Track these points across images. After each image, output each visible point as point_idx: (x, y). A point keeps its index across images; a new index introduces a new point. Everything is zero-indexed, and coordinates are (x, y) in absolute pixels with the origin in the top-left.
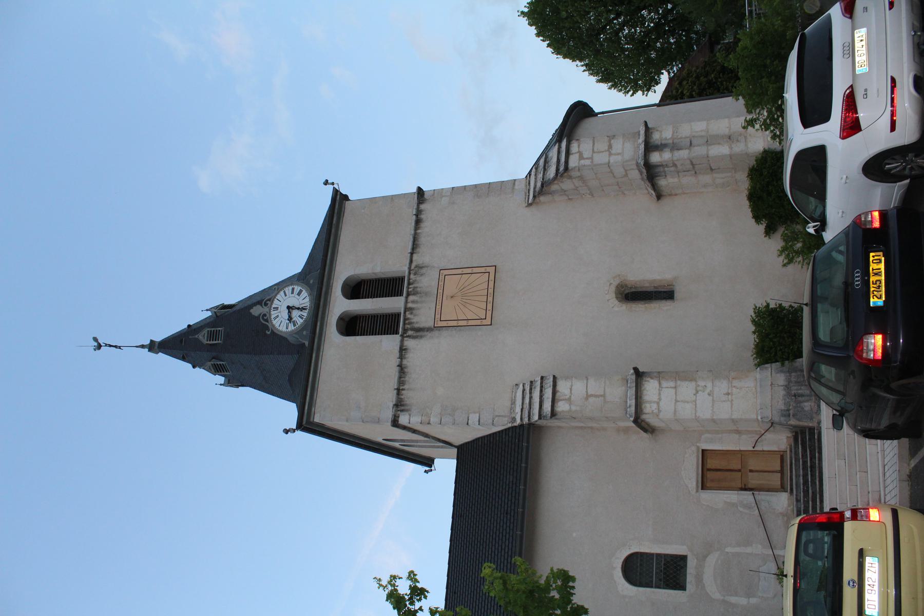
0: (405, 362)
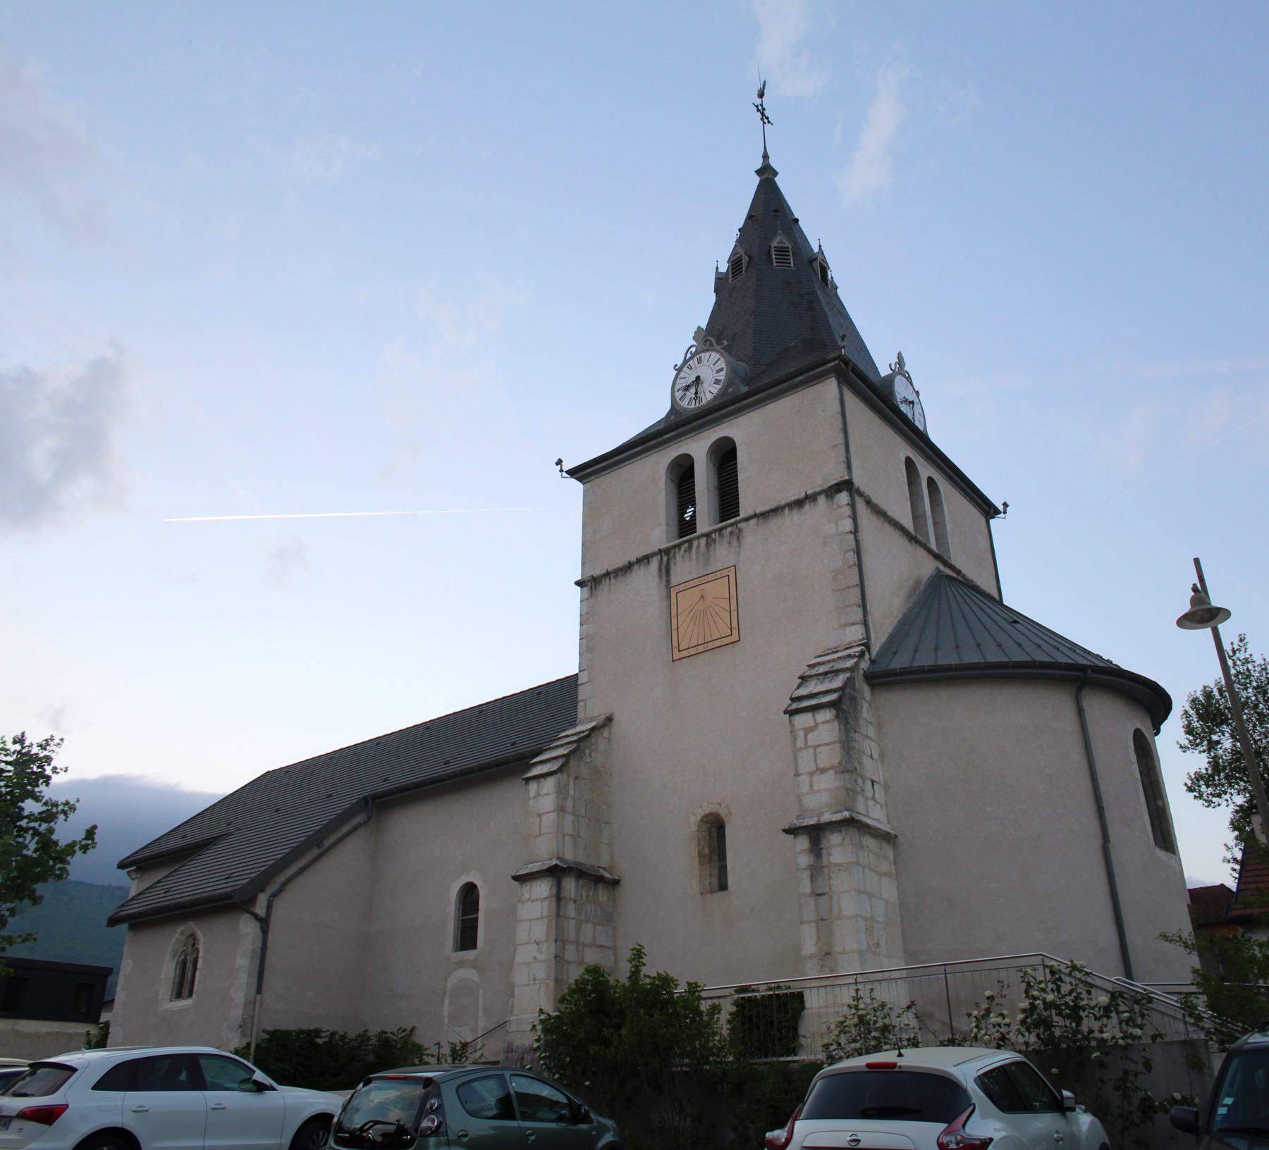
0: (636, 567)
